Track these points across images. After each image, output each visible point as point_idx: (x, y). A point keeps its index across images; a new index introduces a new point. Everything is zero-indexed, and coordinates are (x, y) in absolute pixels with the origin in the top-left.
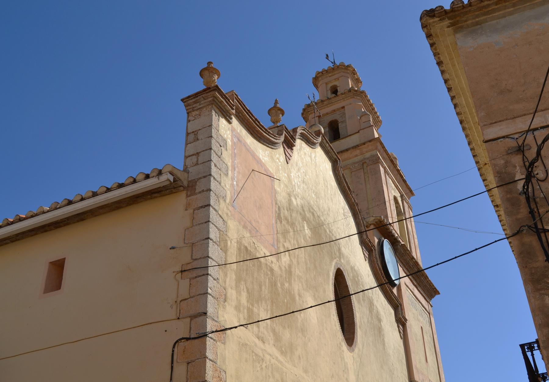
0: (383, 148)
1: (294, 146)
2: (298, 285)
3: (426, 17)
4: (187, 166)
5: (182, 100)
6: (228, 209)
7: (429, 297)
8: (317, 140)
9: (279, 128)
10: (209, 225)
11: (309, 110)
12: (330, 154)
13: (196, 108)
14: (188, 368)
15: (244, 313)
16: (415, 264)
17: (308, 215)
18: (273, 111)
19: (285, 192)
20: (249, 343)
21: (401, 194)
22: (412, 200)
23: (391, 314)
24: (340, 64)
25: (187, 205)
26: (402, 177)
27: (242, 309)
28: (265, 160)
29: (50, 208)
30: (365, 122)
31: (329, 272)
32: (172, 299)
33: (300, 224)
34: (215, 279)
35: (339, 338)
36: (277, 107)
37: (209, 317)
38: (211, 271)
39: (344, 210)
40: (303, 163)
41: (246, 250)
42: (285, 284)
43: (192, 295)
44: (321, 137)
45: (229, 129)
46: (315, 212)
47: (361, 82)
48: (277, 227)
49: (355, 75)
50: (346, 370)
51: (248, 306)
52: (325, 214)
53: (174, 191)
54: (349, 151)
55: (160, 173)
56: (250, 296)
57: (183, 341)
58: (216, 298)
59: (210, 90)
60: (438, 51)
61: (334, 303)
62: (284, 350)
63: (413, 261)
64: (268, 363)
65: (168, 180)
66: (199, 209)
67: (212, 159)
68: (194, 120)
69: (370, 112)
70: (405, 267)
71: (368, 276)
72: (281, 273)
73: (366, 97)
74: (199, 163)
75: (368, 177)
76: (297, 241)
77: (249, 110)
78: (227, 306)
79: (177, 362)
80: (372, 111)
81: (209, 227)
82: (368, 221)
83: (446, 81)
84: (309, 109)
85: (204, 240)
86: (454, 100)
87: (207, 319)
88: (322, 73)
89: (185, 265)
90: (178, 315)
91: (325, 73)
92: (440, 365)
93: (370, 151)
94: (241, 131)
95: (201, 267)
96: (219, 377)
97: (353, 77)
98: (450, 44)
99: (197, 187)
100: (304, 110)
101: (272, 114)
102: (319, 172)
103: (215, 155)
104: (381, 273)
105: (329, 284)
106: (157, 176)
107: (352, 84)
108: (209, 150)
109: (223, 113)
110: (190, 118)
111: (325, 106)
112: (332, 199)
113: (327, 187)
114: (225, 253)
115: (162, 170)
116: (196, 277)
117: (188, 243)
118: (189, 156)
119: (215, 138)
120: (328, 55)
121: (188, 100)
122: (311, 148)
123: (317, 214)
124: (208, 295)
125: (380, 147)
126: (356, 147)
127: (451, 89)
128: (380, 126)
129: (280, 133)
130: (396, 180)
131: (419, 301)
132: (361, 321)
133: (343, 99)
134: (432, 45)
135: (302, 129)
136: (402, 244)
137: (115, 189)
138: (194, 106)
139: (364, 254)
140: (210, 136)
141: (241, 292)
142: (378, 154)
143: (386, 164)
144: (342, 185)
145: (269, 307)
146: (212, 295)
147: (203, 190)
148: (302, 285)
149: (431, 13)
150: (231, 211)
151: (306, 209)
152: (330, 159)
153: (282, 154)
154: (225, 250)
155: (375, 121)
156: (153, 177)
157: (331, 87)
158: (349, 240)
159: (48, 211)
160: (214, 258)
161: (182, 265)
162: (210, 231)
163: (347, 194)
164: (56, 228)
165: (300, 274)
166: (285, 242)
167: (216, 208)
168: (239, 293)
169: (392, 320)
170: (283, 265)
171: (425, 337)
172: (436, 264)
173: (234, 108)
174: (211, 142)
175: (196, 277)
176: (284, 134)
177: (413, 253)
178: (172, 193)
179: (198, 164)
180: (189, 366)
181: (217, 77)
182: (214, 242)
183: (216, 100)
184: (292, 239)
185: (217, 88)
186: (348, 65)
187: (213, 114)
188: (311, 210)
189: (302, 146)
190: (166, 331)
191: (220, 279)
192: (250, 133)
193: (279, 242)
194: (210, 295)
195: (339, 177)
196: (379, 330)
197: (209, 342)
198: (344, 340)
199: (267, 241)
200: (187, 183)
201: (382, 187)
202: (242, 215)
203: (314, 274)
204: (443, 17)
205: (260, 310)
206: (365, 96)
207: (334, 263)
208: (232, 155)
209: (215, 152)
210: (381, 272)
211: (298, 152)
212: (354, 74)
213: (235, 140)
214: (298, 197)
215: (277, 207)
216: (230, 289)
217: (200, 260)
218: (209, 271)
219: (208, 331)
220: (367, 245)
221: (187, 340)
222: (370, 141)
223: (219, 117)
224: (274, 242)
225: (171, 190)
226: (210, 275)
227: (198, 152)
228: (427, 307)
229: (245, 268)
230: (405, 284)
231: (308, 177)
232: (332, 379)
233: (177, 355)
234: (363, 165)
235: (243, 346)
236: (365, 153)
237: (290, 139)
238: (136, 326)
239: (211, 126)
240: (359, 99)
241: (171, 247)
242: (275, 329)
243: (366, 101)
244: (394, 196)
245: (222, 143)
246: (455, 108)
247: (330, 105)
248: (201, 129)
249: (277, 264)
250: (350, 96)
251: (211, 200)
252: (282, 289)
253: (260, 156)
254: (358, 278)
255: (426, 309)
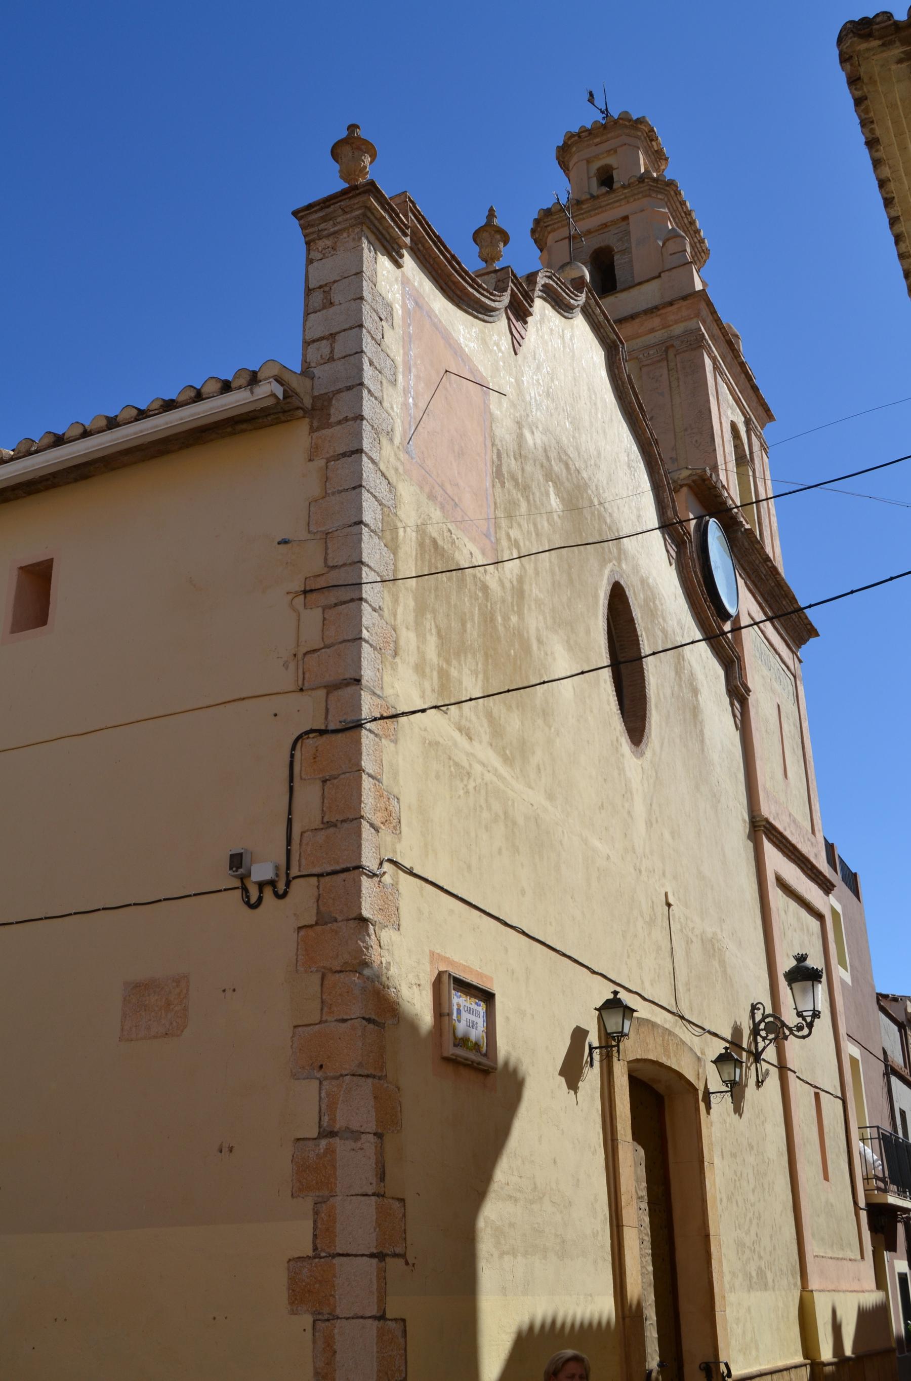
0: (711, 314)
1: (531, 314)
2: (537, 618)
3: (851, 38)
4: (310, 363)
5: (295, 213)
6: (399, 459)
7: (795, 643)
8: (576, 300)
9: (499, 274)
10: (361, 493)
11: (547, 222)
12: (602, 331)
13: (326, 232)
14: (324, 790)
15: (432, 679)
16: (771, 571)
17: (557, 467)
18: (485, 235)
19: (510, 418)
20: (441, 741)
21: (745, 417)
22: (769, 431)
23: (717, 678)
24: (620, 117)
25: (312, 450)
26: (749, 378)
27: (428, 670)
28: (470, 348)
29: (16, 452)
30: (674, 254)
31: (597, 590)
32: (287, 650)
33: (540, 489)
34: (374, 610)
35: (615, 729)
36: (494, 225)
37: (366, 688)
38: (367, 592)
39: (628, 455)
40: (546, 352)
41: (434, 547)
42: (512, 617)
43: (328, 642)
44: (585, 292)
45: (396, 280)
46: (572, 460)
47: (666, 159)
48: (494, 496)
49: (654, 143)
50: (627, 794)
51: (440, 665)
52: (591, 465)
53: (283, 418)
54: (637, 320)
55: (254, 379)
56: (443, 643)
57: (311, 735)
58: (378, 648)
59: (358, 192)
60: (872, 114)
61: (607, 657)
62: (509, 755)
63: (767, 565)
64: (479, 781)
65: (273, 395)
66: (338, 460)
67: (364, 349)
68: (321, 259)
69: (683, 228)
70: (750, 578)
71: (675, 597)
72: (503, 594)
73: (676, 194)
74: (336, 357)
75: (678, 379)
76: (535, 525)
77: (438, 237)
78: (400, 665)
79: (301, 778)
80: (688, 226)
81: (362, 499)
82: (676, 478)
83: (882, 184)
84: (549, 219)
85: (350, 526)
86: (896, 227)
87: (362, 693)
88: (580, 137)
89: (312, 578)
90: (300, 683)
91: (586, 137)
92: (812, 783)
93: (683, 321)
94: (421, 284)
95: (346, 584)
96: (386, 809)
97: (649, 146)
98: (901, 100)
99: (332, 411)
100: (537, 222)
101: (483, 241)
102: (579, 373)
103: (369, 339)
104: (702, 591)
105: (596, 617)
106: (248, 386)
107: (645, 164)
108: (358, 328)
109: (386, 243)
110: (314, 255)
111: (585, 213)
112: (604, 432)
113: (595, 404)
114: (394, 554)
115: (259, 374)
116: (336, 605)
117: (317, 532)
118: (314, 341)
119: (370, 302)
120: (593, 92)
121: (307, 214)
122: (563, 319)
123: (575, 464)
124: (363, 643)
125: (705, 312)
126: (651, 311)
127: (892, 201)
128: (705, 262)
129: (501, 285)
130: (737, 387)
131: (775, 650)
132: (658, 693)
133: (626, 197)
134: (859, 102)
135: (546, 276)
136: (746, 530)
137: (156, 412)
138: (322, 226)
139: (668, 551)
140: (359, 296)
141: (425, 635)
142: (700, 328)
143: (716, 349)
144: (626, 400)
145: (480, 665)
146: (371, 642)
147: (347, 417)
148: (545, 618)
149: (864, 29)
150: (403, 463)
151: (553, 455)
152: (603, 342)
153: (505, 333)
154: (393, 547)
155: (694, 249)
156: (240, 388)
157: (598, 170)
158: (638, 521)
159: (12, 459)
160: (372, 565)
161: (306, 579)
162: (364, 506)
163: (637, 420)
164: (30, 493)
165: (541, 596)
166: (511, 527)
167: (374, 456)
168: (421, 637)
169: (720, 689)
170: (507, 578)
171: (785, 726)
172: (849, 591)
173: (408, 232)
174: (360, 311)
175: (336, 605)
176: (509, 288)
177: (767, 547)
178: (278, 422)
179: (334, 360)
180: (325, 787)
181: (369, 159)
182: (372, 531)
183: (369, 214)
184: (525, 521)
185: (372, 188)
186: (638, 119)
187: (363, 245)
188: (562, 456)
189: (545, 314)
190: (276, 715)
191: (385, 610)
192: (438, 287)
193: (500, 528)
194: (367, 642)
195: (620, 382)
196: (695, 711)
197: (366, 739)
198: (624, 732)
199: (474, 526)
200: (311, 401)
201: (708, 401)
202: (427, 472)
203: (567, 595)
204: (890, 38)
205: (464, 672)
206: (675, 192)
207: (607, 572)
208: (403, 338)
209: (369, 333)
210: (701, 591)
211: (537, 327)
212: (652, 140)
213: (410, 305)
214: (537, 427)
215: (495, 451)
216: (404, 630)
217: (343, 569)
218: (364, 591)
219: (363, 717)
220: (675, 532)
221: (321, 735)
222: (684, 298)
223: (376, 253)
224: (488, 528)
225: (277, 416)
226: (366, 601)
227: (334, 331)
228: (790, 663)
229: (433, 586)
230: (749, 614)
231: (557, 383)
232: (601, 813)
233: (301, 764)
234: (666, 351)
235: (432, 746)
236: (672, 325)
237: (522, 299)
238: (212, 703)
239: (359, 273)
240: (661, 199)
241: (280, 540)
242: (491, 711)
243: (678, 204)
244: (732, 421)
245: (384, 313)
246: (897, 243)
247: (596, 211)
248: (337, 281)
249: (495, 575)
250: (642, 192)
251: (365, 439)
252: (505, 627)
253: (459, 339)
254: (654, 603)
255: (788, 667)
